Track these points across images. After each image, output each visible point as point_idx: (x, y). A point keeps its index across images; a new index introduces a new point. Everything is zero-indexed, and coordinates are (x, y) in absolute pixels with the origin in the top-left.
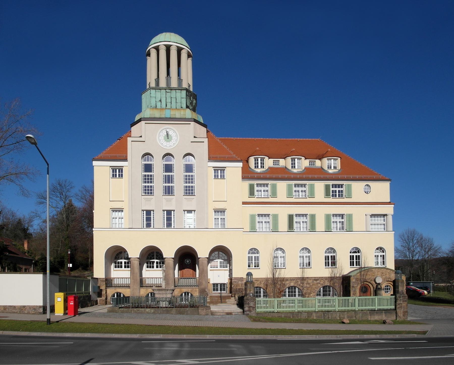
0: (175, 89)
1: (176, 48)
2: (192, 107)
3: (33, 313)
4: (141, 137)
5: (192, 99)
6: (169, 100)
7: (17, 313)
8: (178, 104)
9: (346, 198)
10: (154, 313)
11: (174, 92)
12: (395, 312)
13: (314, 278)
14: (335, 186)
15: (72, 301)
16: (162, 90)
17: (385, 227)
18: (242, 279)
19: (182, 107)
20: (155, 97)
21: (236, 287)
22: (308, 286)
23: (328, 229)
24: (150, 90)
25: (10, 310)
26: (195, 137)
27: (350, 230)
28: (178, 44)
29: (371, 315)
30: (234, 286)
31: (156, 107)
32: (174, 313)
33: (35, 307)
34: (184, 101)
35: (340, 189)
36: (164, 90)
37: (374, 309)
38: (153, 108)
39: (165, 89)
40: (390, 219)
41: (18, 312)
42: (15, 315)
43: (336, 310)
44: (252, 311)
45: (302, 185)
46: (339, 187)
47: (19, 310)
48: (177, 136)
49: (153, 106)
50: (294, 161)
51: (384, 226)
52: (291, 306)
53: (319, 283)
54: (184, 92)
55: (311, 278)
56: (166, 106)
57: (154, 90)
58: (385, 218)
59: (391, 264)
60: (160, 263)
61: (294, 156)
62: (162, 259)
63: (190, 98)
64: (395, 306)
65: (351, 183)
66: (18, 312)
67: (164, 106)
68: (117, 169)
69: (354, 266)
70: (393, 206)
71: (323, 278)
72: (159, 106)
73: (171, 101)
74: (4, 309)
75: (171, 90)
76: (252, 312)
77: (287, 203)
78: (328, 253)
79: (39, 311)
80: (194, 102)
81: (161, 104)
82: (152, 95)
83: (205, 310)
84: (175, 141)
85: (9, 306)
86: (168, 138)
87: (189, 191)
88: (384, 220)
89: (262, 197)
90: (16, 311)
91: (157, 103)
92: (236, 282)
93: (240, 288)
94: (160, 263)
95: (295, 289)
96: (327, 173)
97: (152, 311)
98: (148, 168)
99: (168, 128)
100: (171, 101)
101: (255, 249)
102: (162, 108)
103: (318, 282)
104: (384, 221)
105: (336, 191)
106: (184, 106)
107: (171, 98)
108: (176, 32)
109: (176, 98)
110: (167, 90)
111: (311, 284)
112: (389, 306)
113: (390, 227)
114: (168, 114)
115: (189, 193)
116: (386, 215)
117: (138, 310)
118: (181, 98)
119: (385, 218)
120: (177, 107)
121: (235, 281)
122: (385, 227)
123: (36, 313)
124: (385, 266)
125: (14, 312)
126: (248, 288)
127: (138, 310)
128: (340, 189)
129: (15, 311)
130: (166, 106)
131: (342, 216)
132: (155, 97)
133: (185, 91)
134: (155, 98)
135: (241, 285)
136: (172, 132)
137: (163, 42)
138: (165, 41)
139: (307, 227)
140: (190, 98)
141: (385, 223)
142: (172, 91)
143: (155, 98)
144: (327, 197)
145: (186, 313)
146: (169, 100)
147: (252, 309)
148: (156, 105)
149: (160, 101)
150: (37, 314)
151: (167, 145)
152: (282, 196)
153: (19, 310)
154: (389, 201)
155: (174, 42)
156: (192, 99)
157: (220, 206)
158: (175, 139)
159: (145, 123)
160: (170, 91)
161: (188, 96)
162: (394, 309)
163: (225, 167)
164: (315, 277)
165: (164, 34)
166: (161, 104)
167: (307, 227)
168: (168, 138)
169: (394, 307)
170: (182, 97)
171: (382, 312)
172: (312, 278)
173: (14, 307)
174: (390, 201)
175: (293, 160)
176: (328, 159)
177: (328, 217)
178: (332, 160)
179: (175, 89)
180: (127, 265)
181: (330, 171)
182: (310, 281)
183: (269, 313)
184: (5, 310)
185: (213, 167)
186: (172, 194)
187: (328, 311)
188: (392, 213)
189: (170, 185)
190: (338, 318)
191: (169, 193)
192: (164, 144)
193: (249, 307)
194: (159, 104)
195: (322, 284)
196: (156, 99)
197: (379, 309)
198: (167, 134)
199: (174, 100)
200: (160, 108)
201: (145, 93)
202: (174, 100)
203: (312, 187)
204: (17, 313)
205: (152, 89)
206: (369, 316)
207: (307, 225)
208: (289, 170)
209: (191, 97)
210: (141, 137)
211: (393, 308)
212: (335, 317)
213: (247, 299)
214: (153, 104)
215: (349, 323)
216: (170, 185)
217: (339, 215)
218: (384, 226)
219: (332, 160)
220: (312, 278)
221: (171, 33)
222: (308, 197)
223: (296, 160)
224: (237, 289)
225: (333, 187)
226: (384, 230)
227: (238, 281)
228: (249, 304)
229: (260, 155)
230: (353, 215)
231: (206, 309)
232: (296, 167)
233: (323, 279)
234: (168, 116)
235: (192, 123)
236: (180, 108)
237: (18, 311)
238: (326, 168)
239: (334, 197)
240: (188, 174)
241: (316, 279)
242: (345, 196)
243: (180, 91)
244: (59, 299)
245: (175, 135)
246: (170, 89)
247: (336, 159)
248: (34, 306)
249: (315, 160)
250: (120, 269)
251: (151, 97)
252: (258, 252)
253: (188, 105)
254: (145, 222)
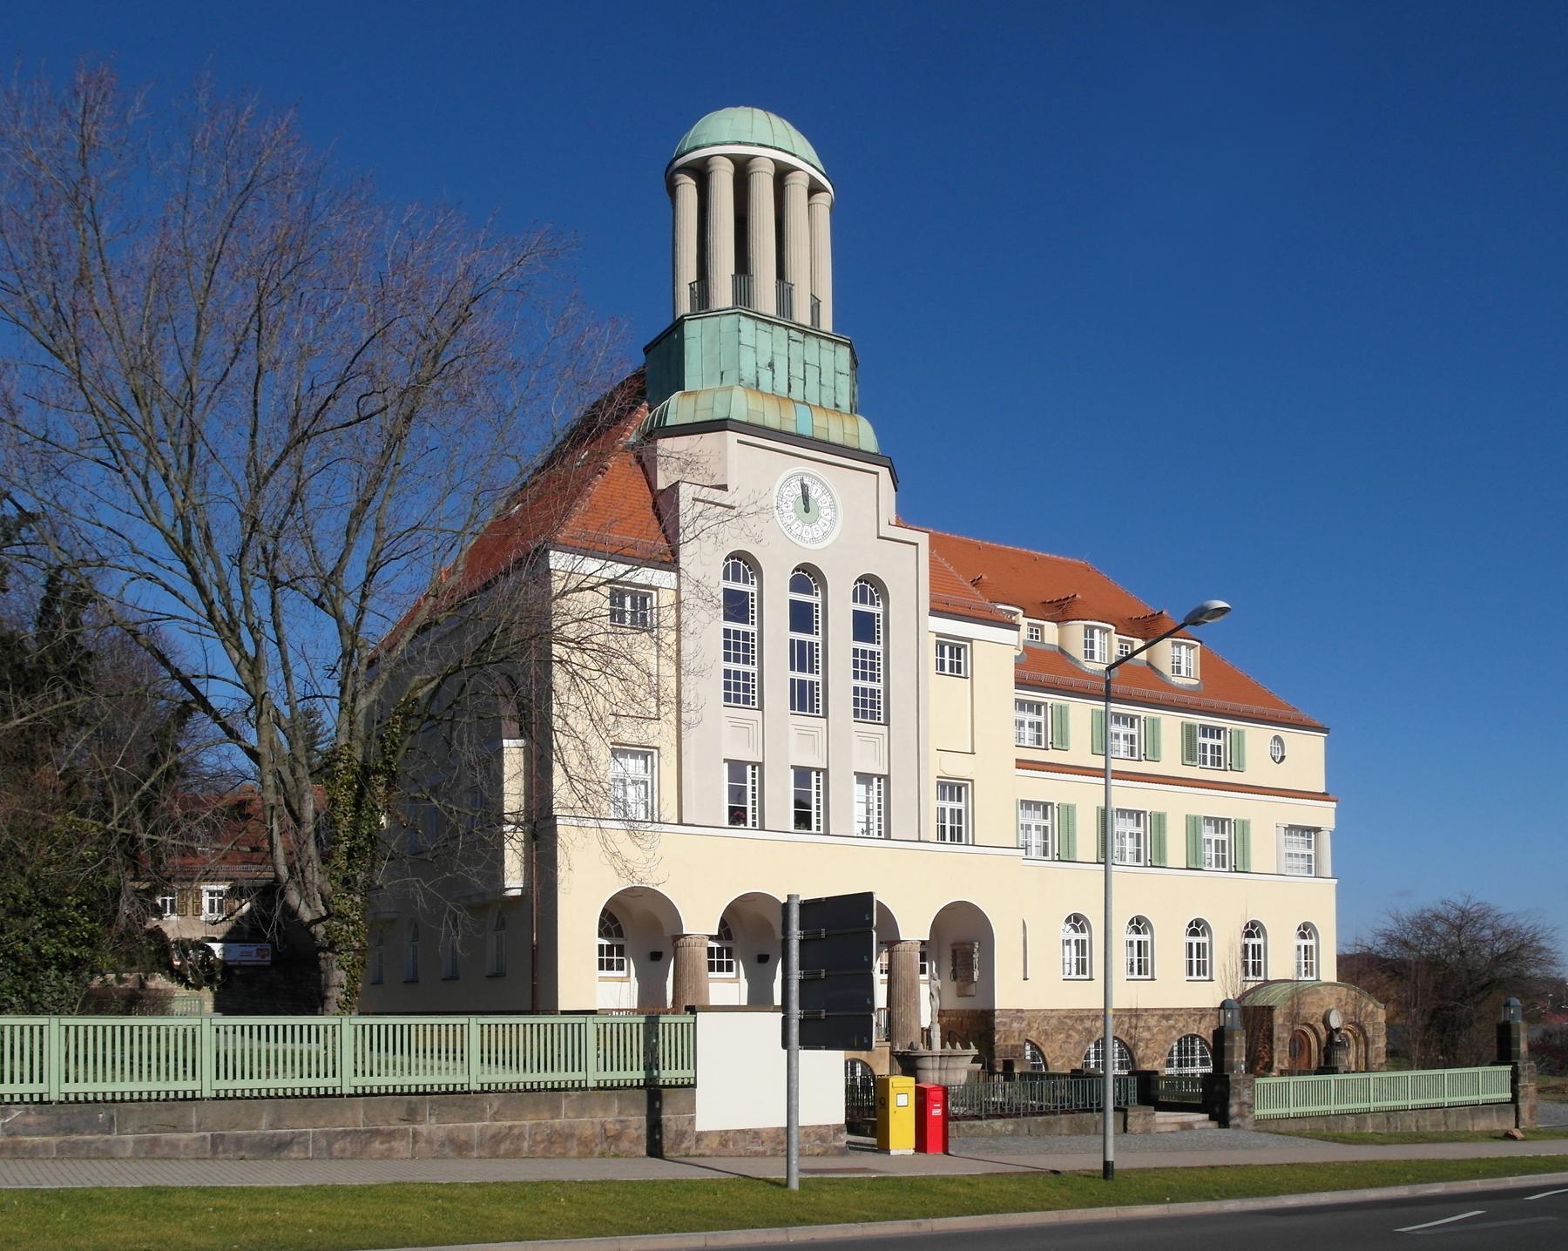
1: (771, 169)
3: (817, 1151)
6: (797, 371)
7: (763, 1154)
9: (1231, 770)
10: (1014, 1133)
12: (1512, 1107)
13: (1161, 1012)
14: (1208, 731)
15: (936, 1102)
17: (1313, 864)
18: (1019, 1014)
19: (837, 406)
20: (755, 349)
21: (1005, 1041)
22: (1146, 1035)
23: (1193, 865)
25: (741, 1144)
27: (1241, 868)
28: (783, 154)
29: (1473, 1119)
30: (1000, 1038)
31: (758, 385)
32: (1065, 1132)
33: (824, 1131)
34: (845, 384)
35: (1216, 742)
36: (782, 329)
37: (580, 1082)
40: (1325, 838)
41: (769, 1153)
42: (759, 1161)
43: (204, 1095)
44: (1246, 1117)
46: (1212, 736)
47: (773, 1145)
48: (833, 506)
50: (1092, 636)
51: (1310, 861)
53: (1174, 1027)
55: (1154, 1013)
56: (789, 391)
57: (751, 322)
58: (1313, 839)
59: (1328, 971)
60: (610, 953)
61: (1095, 620)
62: (617, 936)
64: (1514, 1091)
65: (1158, 716)
66: (769, 1153)
67: (782, 388)
68: (947, 643)
70: (1334, 804)
71: (1182, 1012)
72: (766, 385)
74: (721, 1144)
76: (1247, 1120)
77: (1224, 786)
79: (837, 1144)
81: (773, 378)
83: (1142, 1117)
84: (828, 523)
85: (738, 1131)
86: (807, 510)
87: (869, 707)
88: (1309, 842)
89: (1122, 756)
90: (761, 1149)
91: (760, 370)
92: (1005, 1024)
93: (1017, 1043)
94: (610, 953)
95: (1193, 1043)
96: (1075, 669)
97: (1010, 1127)
99: (807, 475)
103: (1172, 1022)
104: (1309, 847)
107: (805, 364)
108: (767, 106)
111: (1155, 1030)
112: (632, 1069)
113: (1327, 867)
114: (801, 421)
115: (864, 713)
116: (1317, 830)
117: (972, 1127)
118: (835, 372)
119: (1313, 839)
121: (1004, 1020)
122: (1313, 864)
123: (830, 1152)
124: (1314, 978)
125: (756, 1154)
126: (1235, 1048)
127: (972, 1127)
128: (1216, 742)
129: (757, 1148)
130: (789, 391)
131: (1044, 807)
132: (755, 349)
134: (755, 352)
135: (1017, 1034)
136: (820, 492)
137: (771, 147)
138: (780, 149)
139: (1138, 851)
141: (1312, 852)
143: (755, 352)
144: (1189, 762)
145: (1093, 1131)
146: (797, 371)
147: (1246, 1110)
148: (757, 379)
149: (771, 365)
150: (832, 1155)
151: (804, 535)
152: (1258, 768)
153: (773, 1145)
154: (1322, 789)
155: (807, 162)
157: (957, 768)
159: (739, 442)
162: (642, 1083)
163: (970, 640)
164: (1163, 1009)
165: (759, 113)
166: (773, 378)
167: (1138, 851)
168: (807, 510)
169: (1510, 1095)
170: (838, 369)
171: (1491, 1109)
172: (1157, 1012)
173: (756, 1134)
174: (1323, 791)
175: (1089, 631)
176: (1174, 644)
177: (1193, 824)
178: (1184, 647)
180: (725, 960)
181: (1176, 680)
182: (1152, 1022)
183: (32, 1106)
184: (724, 1146)
185: (938, 635)
186: (812, 710)
187: (1396, 1111)
188: (1332, 826)
190: (1414, 1130)
191: (802, 708)
192: (793, 527)
193: (1242, 1104)
195: (1180, 1031)
196: (759, 355)
197: (486, 1088)
198: (806, 497)
200: (770, 392)
201: (705, 320)
203: (1062, 714)
204: (763, 1154)
206: (1470, 1121)
207: (1138, 845)
208: (1078, 661)
211: (638, 1080)
212: (1410, 1126)
213: (1237, 1082)
214: (748, 373)
215: (1523, 1140)
217: (1037, 805)
218: (1310, 861)
219: (1184, 647)
220: (1157, 1012)
221: (755, 110)
222: (1050, 746)
223: (1097, 632)
224: (1007, 1046)
225: (1205, 735)
226: (1310, 872)
227: (1011, 1022)
228: (1239, 1095)
229: (1008, 604)
230: (1251, 825)
231: (1145, 1115)
232: (1097, 658)
233: (1181, 1015)
236: (833, 408)
237: (768, 1147)
238: (1166, 668)
239: (741, 705)
240: (733, 626)
241: (1167, 1015)
242: (1052, 743)
243: (831, 346)
244: (902, 1100)
245: (828, 504)
246: (799, 331)
247: (1194, 647)
248: (820, 1126)
249: (1132, 639)
250: (725, 974)
251: (740, 343)
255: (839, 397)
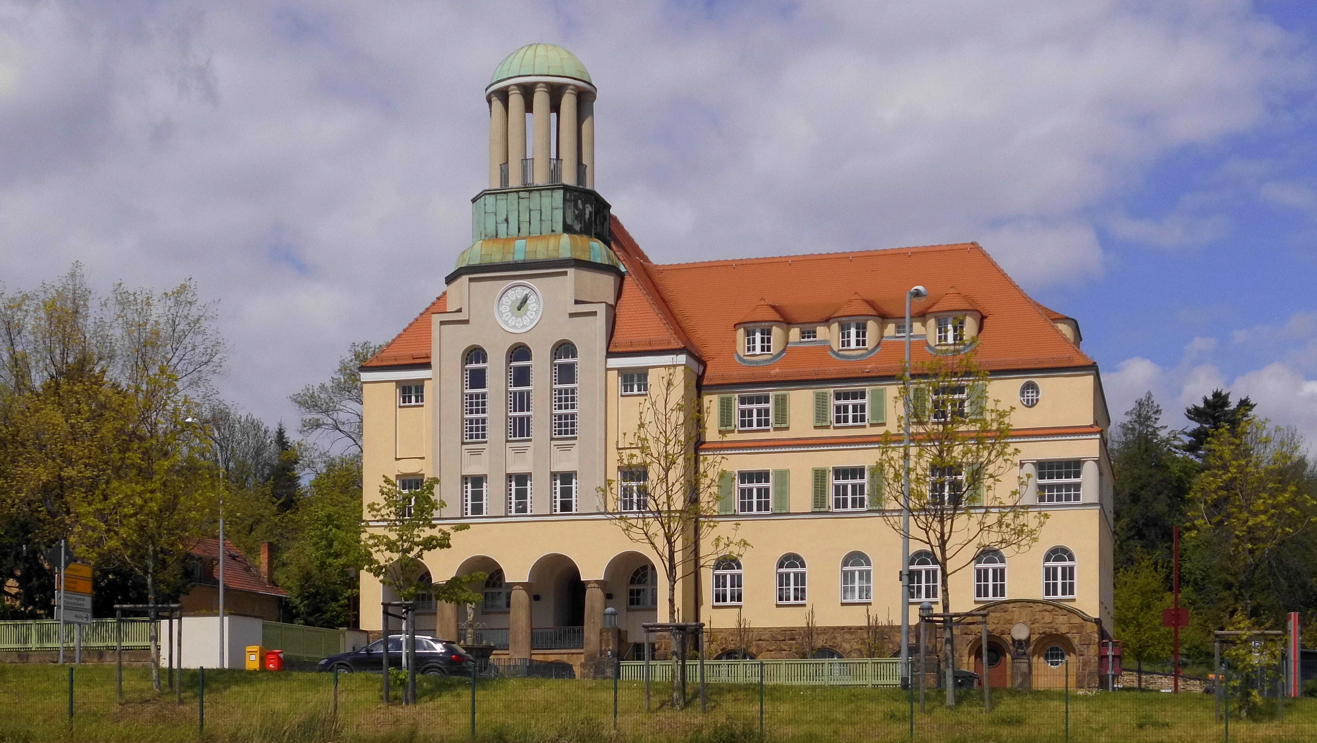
0: (539, 190)
2: (581, 223)
4: (460, 311)
5: (580, 206)
6: (525, 217)
8: (544, 225)
11: (536, 195)
16: (510, 195)
19: (553, 231)
24: (483, 197)
26: (577, 302)
31: (497, 235)
34: (559, 215)
38: (490, 239)
39: (517, 192)
45: (855, 395)
49: (490, 235)
52: (69, 603)
54: (559, 195)
57: (493, 197)
63: (576, 206)
69: (987, 596)
73: (530, 220)
75: (530, 191)
78: (1053, 561)
80: (587, 212)
81: (508, 227)
82: (490, 208)
84: (534, 313)
98: (478, 379)
100: (530, 220)
101: (1065, 550)
102: (509, 237)
105: (846, 408)
106: (559, 227)
107: (530, 210)
109: (541, 210)
110: (521, 194)
120: (543, 232)
130: (519, 231)
133: (562, 191)
134: (496, 215)
138: (520, 76)
140: (576, 206)
142: (532, 194)
143: (496, 215)
146: (525, 217)
149: (507, 220)
156: (580, 206)
158: (535, 309)
160: (526, 195)
161: (570, 201)
166: (508, 227)
179: (539, 190)
188: (1096, 454)
189: (525, 413)
194: (502, 228)
199: (535, 216)
202: (535, 216)
205: (489, 194)
209: (580, 202)
210: (460, 311)
214: (491, 229)
216: (525, 413)
234: (519, 257)
235: (571, 271)
243: (549, 192)
252: (1071, 558)
253: (569, 222)
254: (513, 501)
255: (555, 225)
